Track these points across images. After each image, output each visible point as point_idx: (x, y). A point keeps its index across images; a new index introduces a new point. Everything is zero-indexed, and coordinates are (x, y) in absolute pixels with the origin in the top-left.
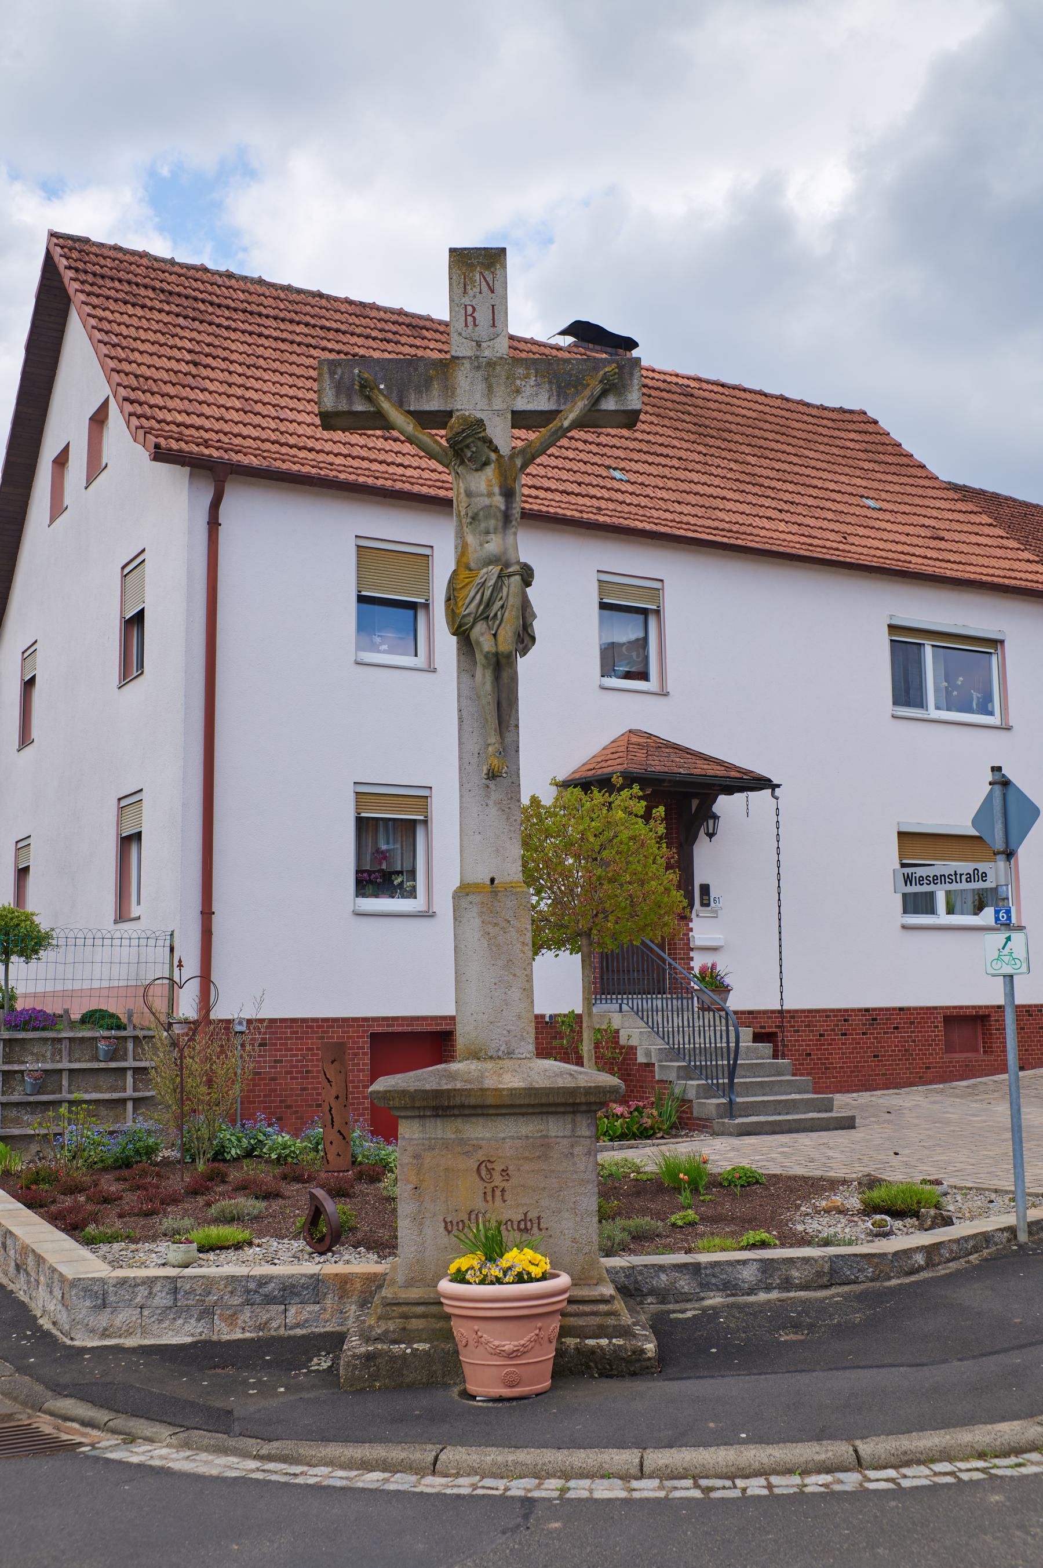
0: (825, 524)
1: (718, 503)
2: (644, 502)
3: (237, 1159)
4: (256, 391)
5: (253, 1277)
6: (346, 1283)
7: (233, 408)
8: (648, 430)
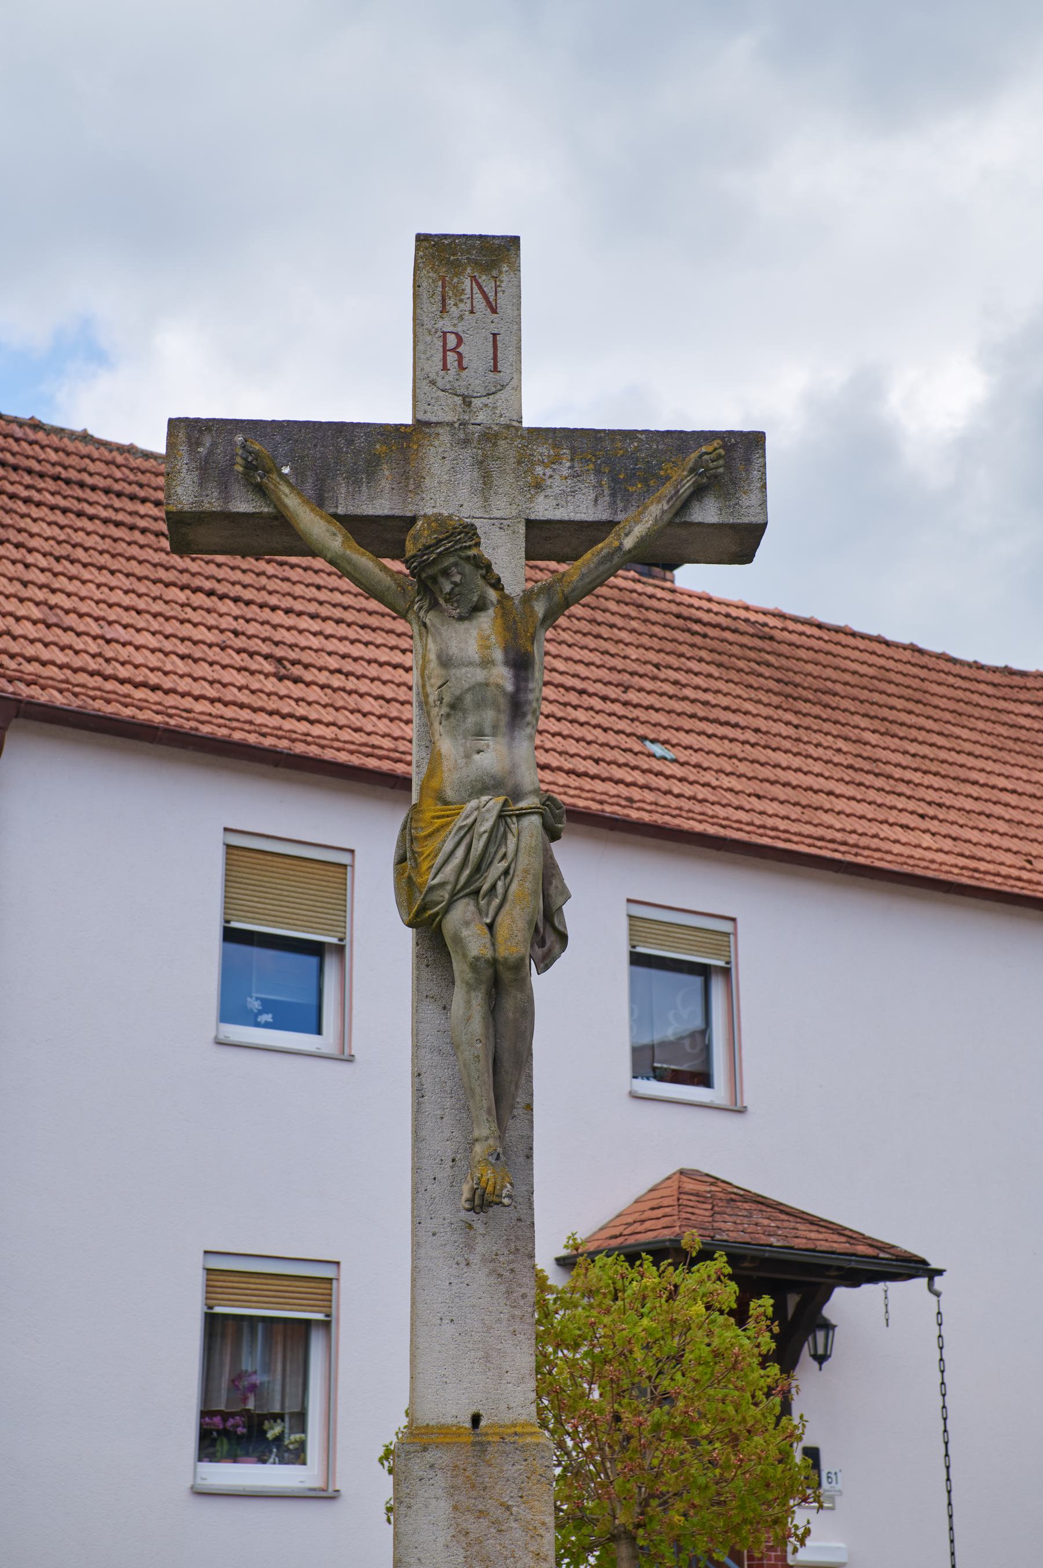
0: (996, 840)
1: (821, 800)
2: (702, 793)
4: (69, 595)
7: (28, 619)
8: (704, 685)
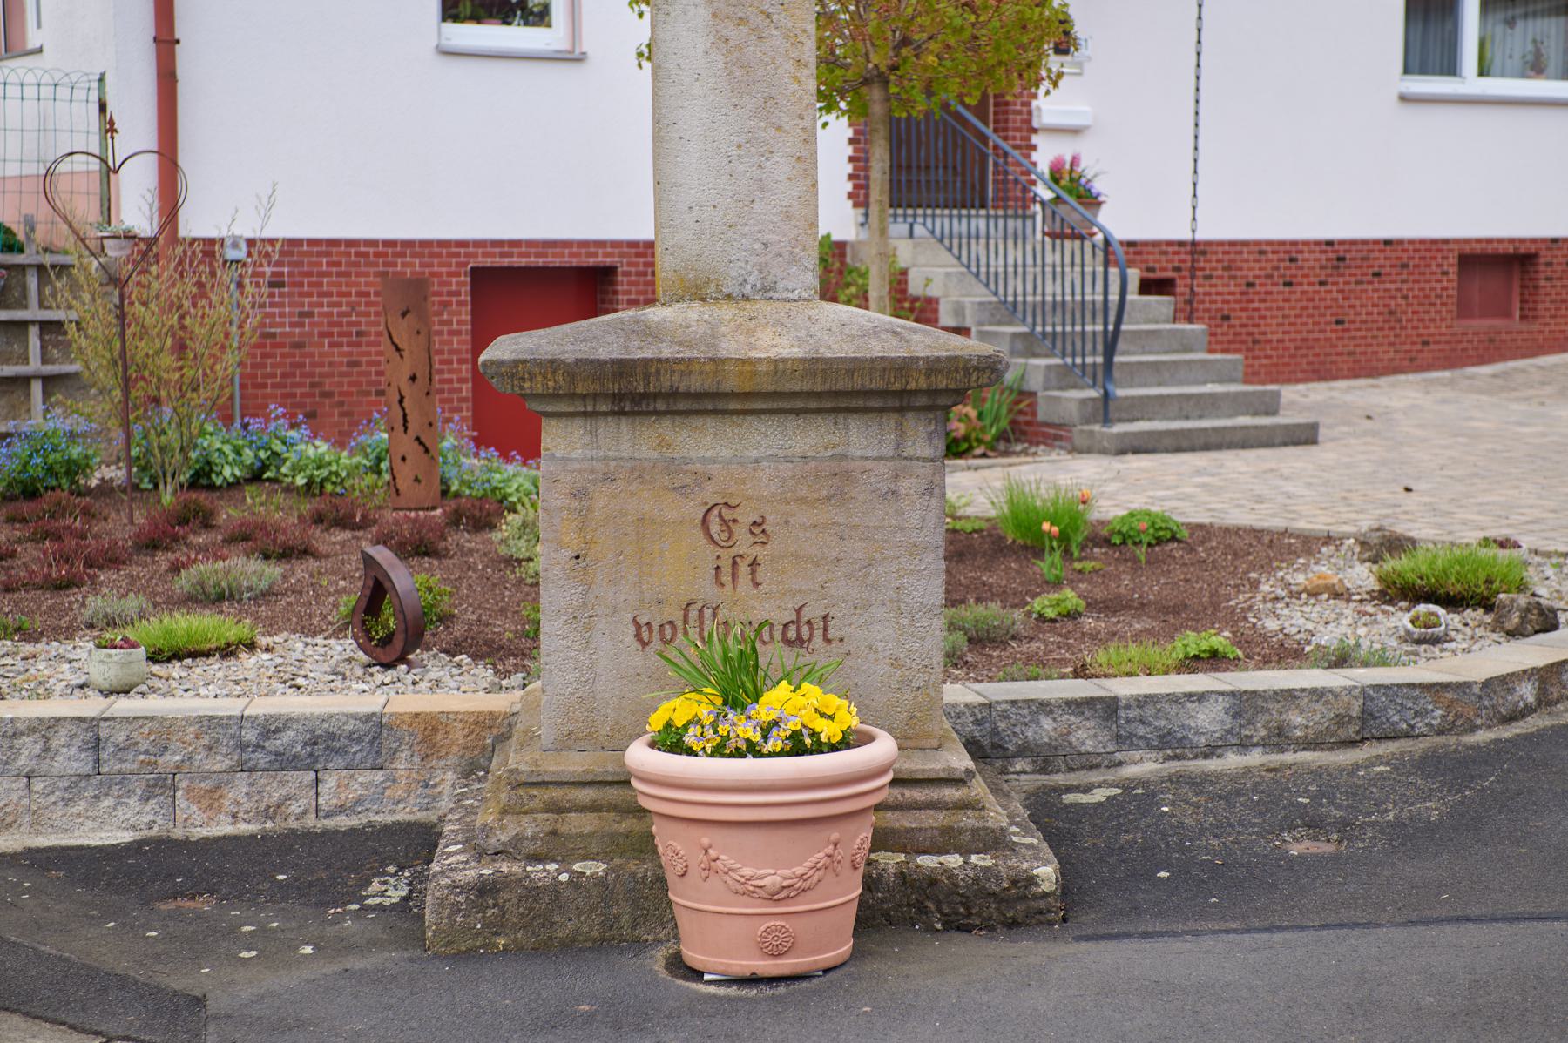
3: (236, 484)
5: (252, 719)
6: (435, 730)
